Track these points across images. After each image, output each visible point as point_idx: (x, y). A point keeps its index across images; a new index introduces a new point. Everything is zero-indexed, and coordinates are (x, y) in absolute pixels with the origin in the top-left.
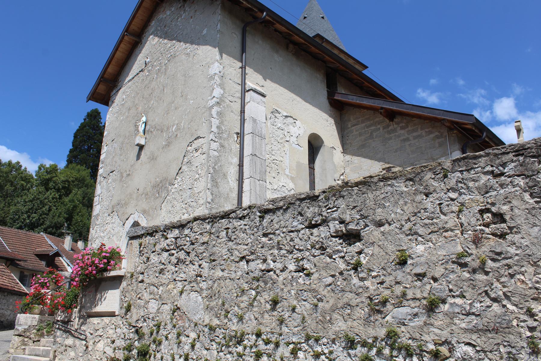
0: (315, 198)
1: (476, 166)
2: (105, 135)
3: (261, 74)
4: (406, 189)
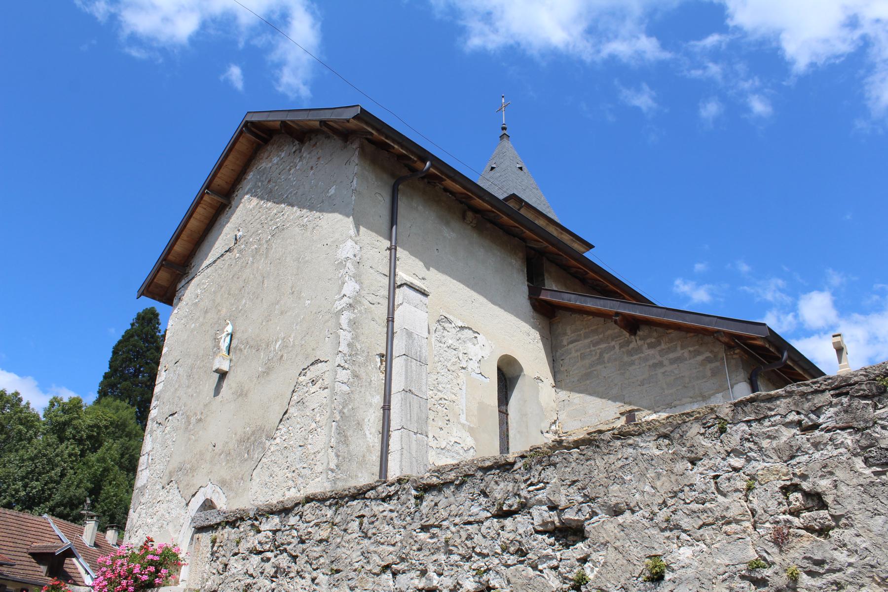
0: (508, 467)
1: (773, 413)
4: (658, 452)
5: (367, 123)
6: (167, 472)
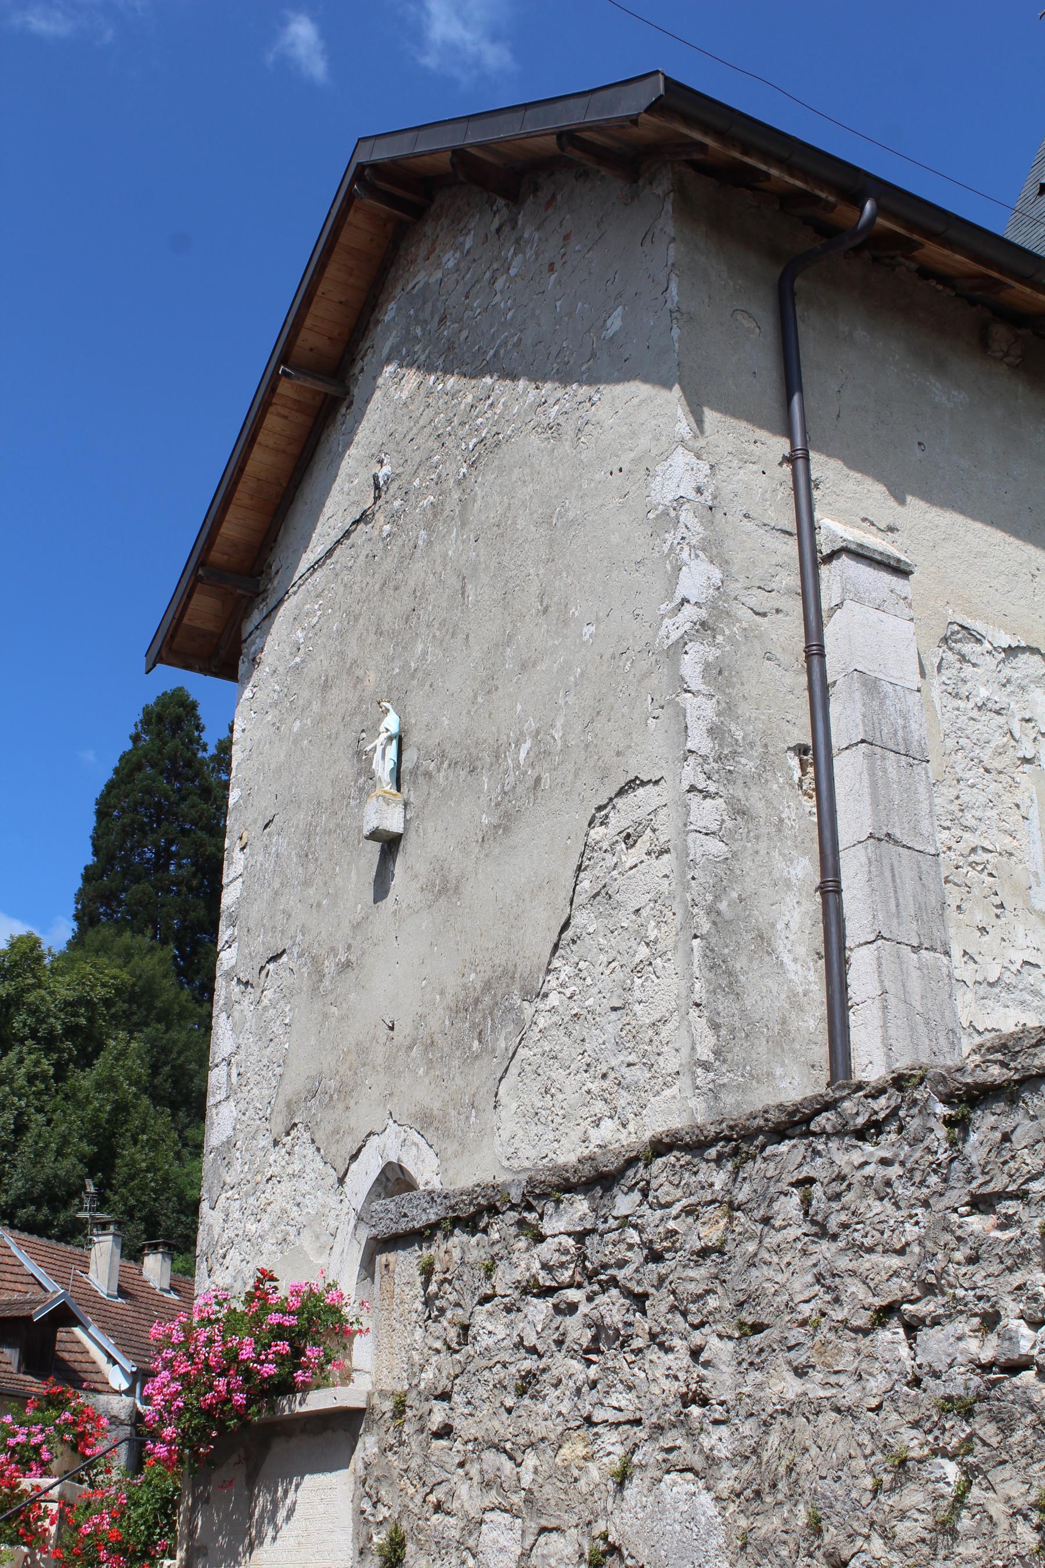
2: (231, 802)
3: (879, 478)
5: (687, 119)
6: (281, 1104)
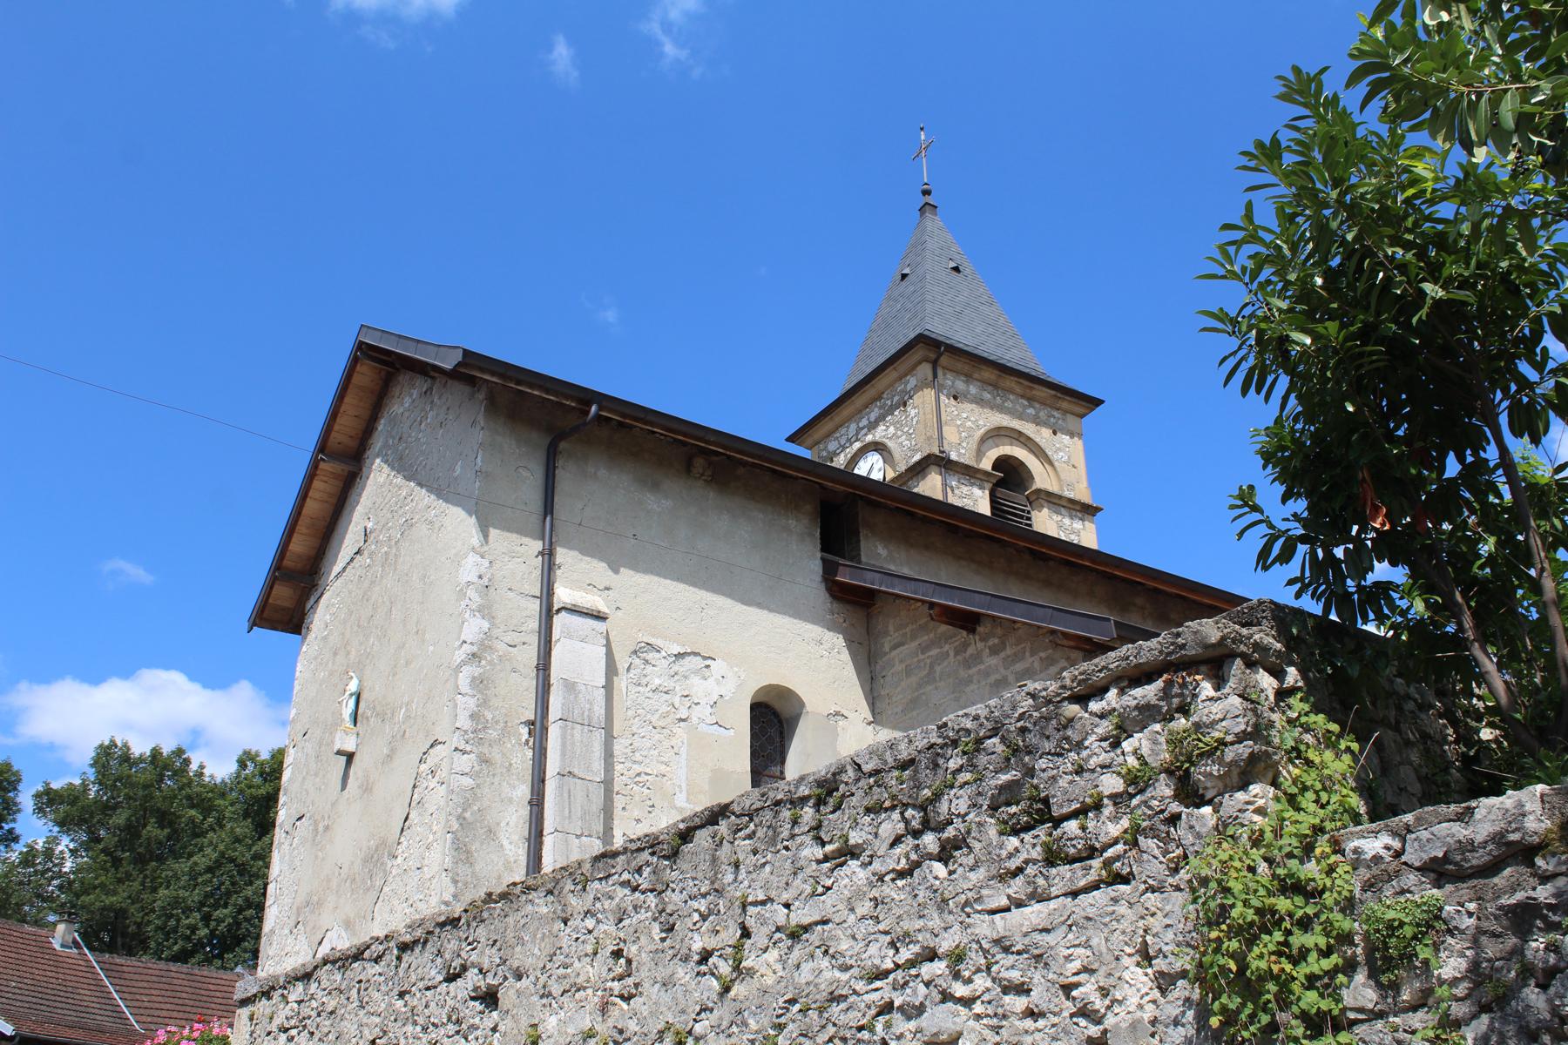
3: (602, 559)
